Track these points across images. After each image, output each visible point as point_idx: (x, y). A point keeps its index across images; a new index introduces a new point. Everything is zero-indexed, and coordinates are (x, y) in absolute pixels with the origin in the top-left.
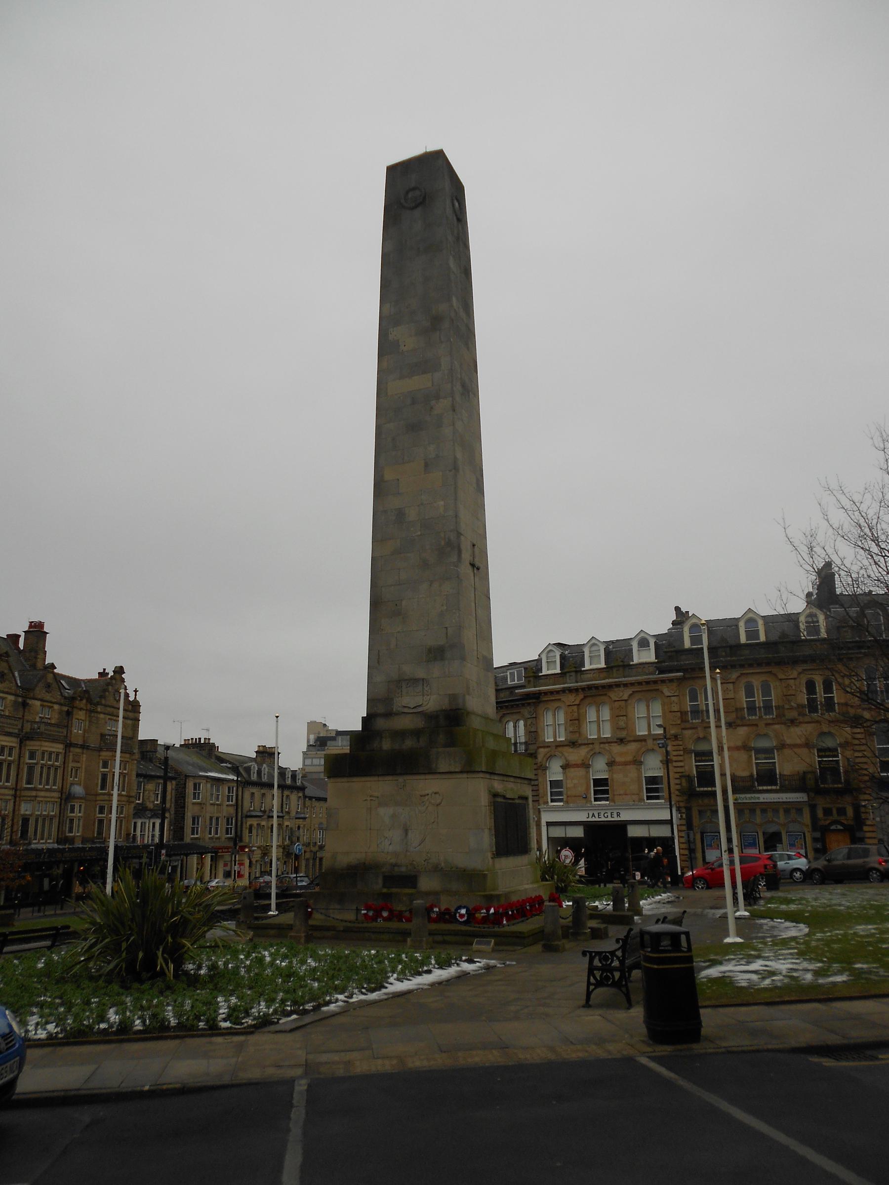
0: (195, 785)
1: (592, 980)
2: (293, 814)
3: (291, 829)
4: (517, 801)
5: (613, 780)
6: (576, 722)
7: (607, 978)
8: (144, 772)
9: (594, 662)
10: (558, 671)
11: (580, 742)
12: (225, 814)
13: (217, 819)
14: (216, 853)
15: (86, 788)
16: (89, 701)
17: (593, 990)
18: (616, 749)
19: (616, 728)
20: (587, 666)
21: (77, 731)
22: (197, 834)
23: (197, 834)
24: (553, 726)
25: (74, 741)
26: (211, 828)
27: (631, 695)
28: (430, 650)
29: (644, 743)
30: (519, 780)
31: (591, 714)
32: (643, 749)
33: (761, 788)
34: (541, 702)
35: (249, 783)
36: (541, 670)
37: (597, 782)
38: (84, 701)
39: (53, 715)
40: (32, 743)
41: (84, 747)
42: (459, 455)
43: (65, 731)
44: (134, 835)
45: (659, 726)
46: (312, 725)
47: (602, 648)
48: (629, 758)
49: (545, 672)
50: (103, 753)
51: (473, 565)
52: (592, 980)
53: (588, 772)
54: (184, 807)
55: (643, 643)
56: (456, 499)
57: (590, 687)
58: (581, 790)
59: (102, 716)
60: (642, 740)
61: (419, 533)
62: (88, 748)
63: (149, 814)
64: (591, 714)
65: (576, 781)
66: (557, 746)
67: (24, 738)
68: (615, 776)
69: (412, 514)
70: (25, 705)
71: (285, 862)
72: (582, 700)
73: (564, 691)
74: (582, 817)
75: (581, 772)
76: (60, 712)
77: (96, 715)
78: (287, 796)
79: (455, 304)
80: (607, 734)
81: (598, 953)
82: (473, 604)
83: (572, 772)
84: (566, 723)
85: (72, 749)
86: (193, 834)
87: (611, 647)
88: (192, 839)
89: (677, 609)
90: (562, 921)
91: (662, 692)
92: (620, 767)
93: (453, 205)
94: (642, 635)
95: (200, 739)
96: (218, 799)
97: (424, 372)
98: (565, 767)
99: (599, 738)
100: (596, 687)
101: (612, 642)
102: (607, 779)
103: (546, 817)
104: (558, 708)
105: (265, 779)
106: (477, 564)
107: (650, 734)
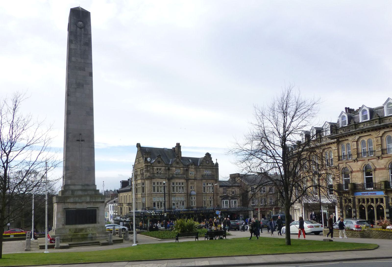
25: (190, 178)
33: (369, 189)
38: (193, 165)
39: (180, 171)
40: (173, 180)
41: (195, 179)
50: (203, 181)
59: (202, 169)
62: (196, 180)
67: (169, 179)
70: (169, 169)
76: (184, 170)
89: (138, 145)
103: (225, 207)
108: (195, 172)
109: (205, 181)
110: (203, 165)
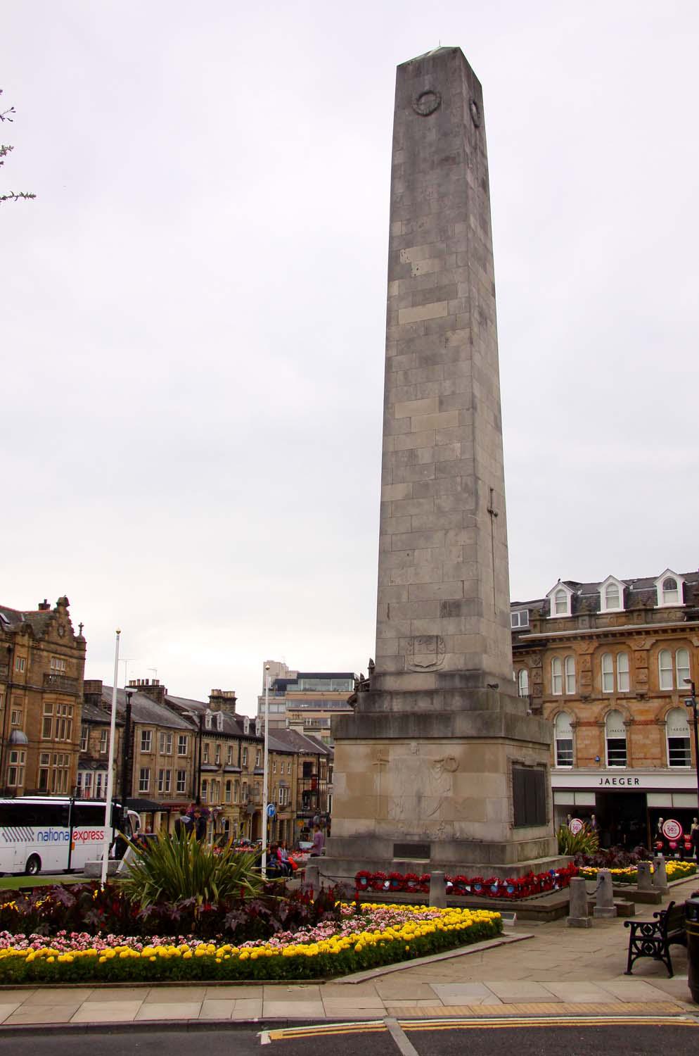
0: (144, 733)
1: (634, 950)
2: (251, 769)
3: (249, 786)
4: (535, 768)
5: (631, 741)
6: (588, 674)
7: (649, 948)
8: (89, 718)
9: (612, 605)
10: (569, 614)
11: (593, 696)
12: (176, 767)
13: (168, 772)
14: (169, 811)
15: (28, 734)
16: (32, 635)
17: (635, 959)
18: (636, 706)
19: (636, 682)
20: (603, 610)
21: (19, 669)
22: (146, 789)
23: (146, 789)
24: (563, 677)
26: (161, 783)
27: (653, 645)
28: (444, 605)
29: (668, 700)
30: (537, 746)
31: (607, 665)
32: (668, 707)
34: (547, 650)
35: (202, 733)
36: (548, 612)
37: (613, 744)
41: (25, 688)
42: (477, 394)
43: (6, 670)
44: (79, 789)
45: (687, 681)
46: (269, 667)
47: (621, 588)
48: (651, 717)
49: (553, 615)
50: (46, 696)
51: (491, 512)
52: (634, 950)
53: (602, 732)
54: (132, 758)
55: (670, 585)
56: (474, 440)
57: (606, 635)
58: (593, 751)
59: (45, 654)
60: (666, 696)
61: (433, 477)
63: (94, 765)
64: (607, 665)
65: (589, 743)
66: (566, 701)
68: (634, 737)
69: (425, 457)
71: (242, 825)
72: (597, 648)
73: (575, 637)
74: (594, 782)
75: (594, 731)
77: (39, 652)
78: (246, 748)
79: (473, 226)
80: (625, 688)
81: (640, 925)
82: (491, 555)
83: (584, 731)
84: (577, 674)
85: (13, 690)
86: (141, 788)
87: (631, 587)
88: (140, 794)
90: (588, 897)
91: (691, 642)
92: (641, 727)
93: (471, 110)
94: (669, 574)
95: (147, 681)
96: (168, 750)
97: (439, 300)
98: (575, 725)
99: (616, 692)
100: (614, 635)
101: (633, 581)
102: (624, 740)
104: (569, 657)
105: (258, 734)
106: (495, 510)
107: (675, 690)
108: (30, 662)
109: (54, 696)
110: (51, 640)
